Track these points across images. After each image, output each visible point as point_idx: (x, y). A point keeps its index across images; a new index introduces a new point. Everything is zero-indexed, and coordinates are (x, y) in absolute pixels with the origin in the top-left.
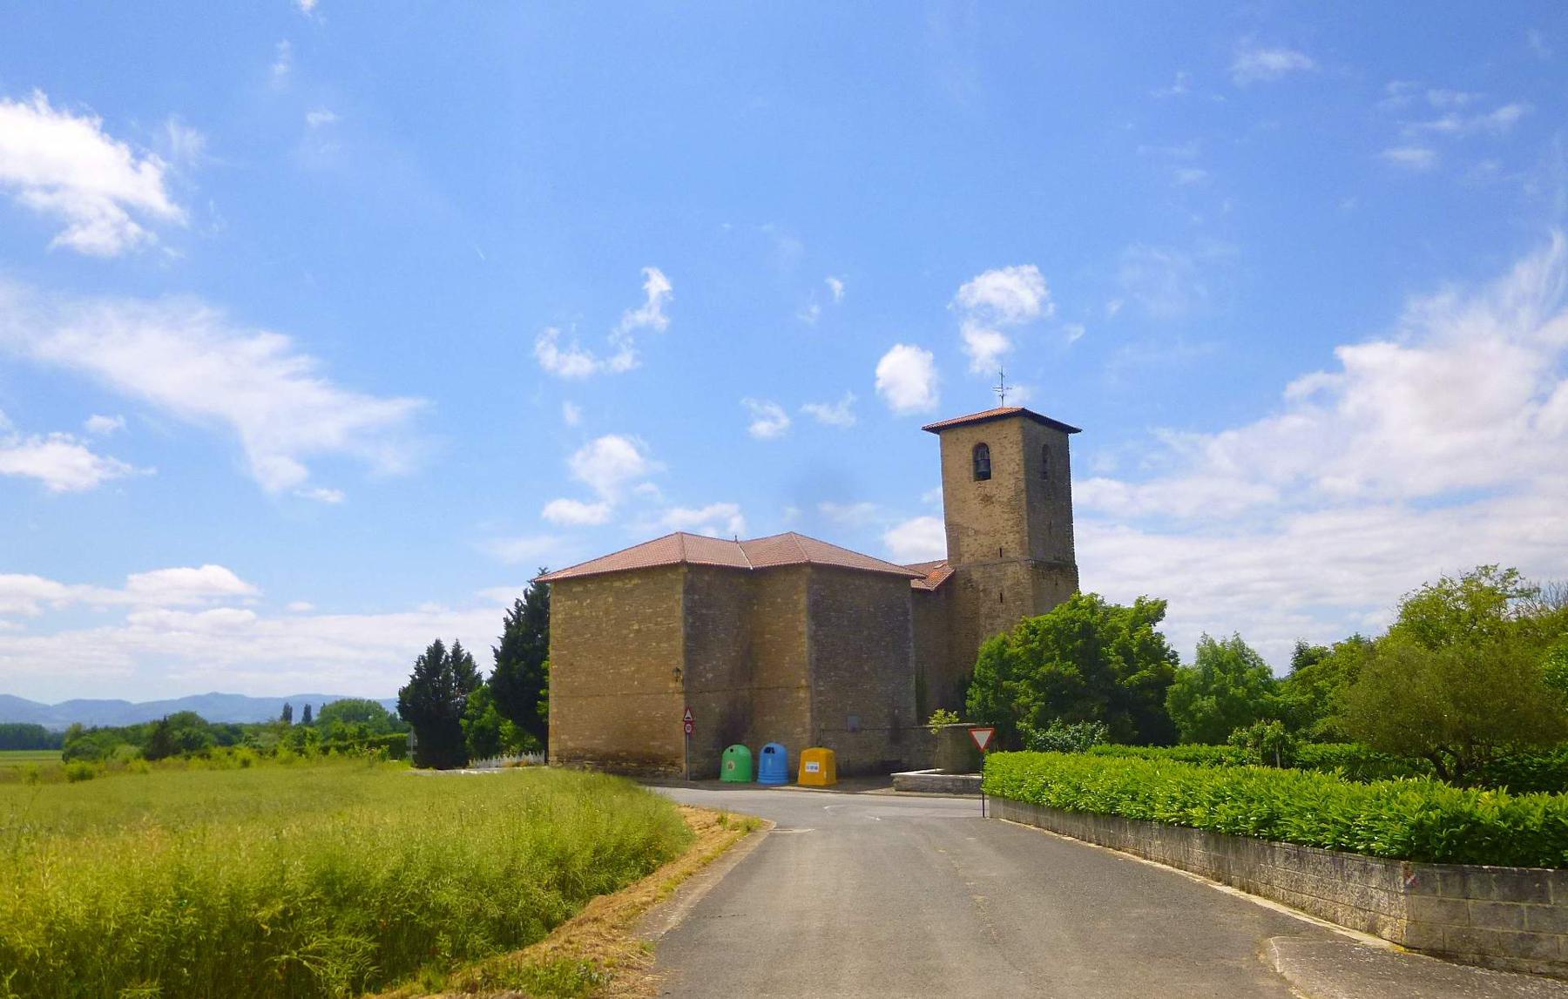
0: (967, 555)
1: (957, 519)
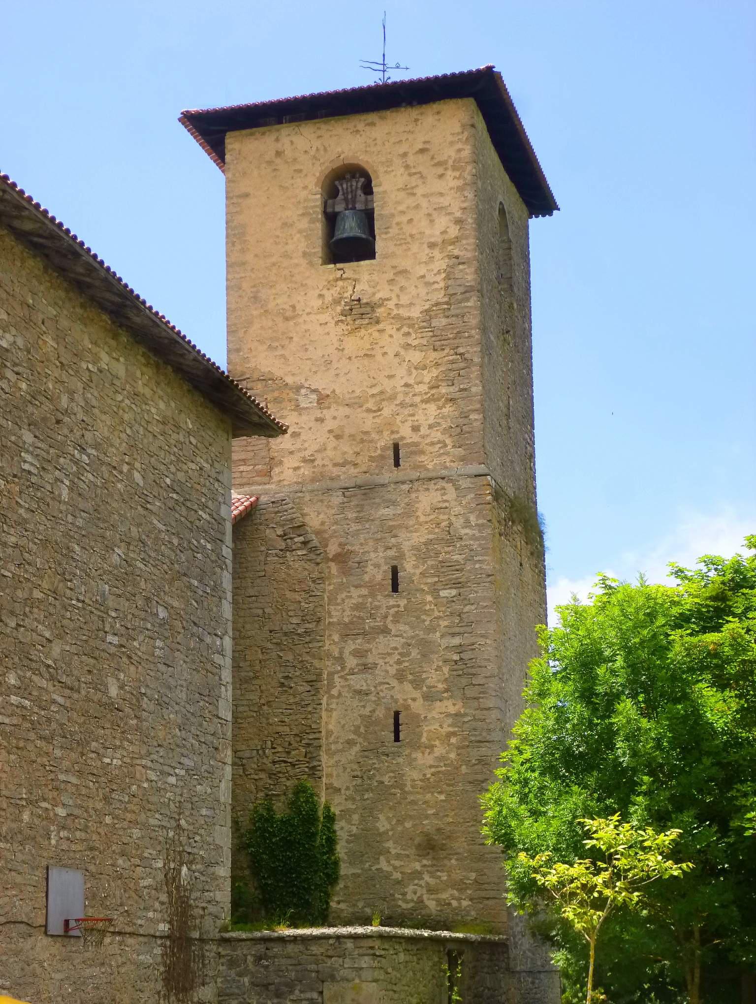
0: (290, 462)
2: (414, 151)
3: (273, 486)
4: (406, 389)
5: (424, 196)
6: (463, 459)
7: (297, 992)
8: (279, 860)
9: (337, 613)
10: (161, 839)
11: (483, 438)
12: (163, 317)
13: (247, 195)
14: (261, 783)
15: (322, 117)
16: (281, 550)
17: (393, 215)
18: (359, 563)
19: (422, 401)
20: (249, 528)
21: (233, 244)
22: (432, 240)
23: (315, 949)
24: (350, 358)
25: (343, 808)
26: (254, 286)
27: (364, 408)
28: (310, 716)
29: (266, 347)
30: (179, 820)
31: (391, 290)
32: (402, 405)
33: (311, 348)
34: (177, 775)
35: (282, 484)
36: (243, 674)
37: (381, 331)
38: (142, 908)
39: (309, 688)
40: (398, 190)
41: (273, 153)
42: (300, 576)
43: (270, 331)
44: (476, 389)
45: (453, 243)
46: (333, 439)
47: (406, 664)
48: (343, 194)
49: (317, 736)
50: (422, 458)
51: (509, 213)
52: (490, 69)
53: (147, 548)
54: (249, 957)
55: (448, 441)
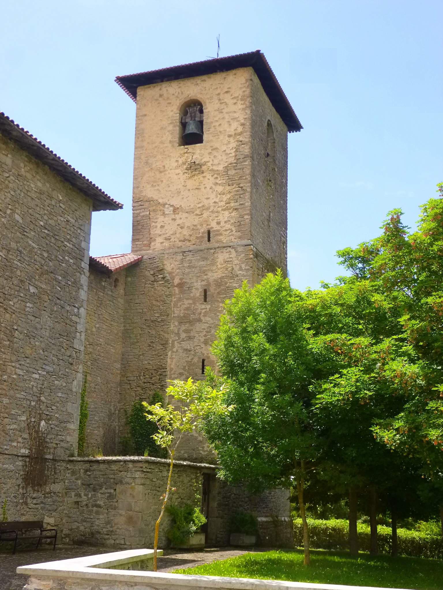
0: (159, 240)
1: (150, 193)
2: (223, 92)
3: (151, 251)
4: (215, 204)
5: (227, 113)
6: (240, 238)
7: (104, 489)
8: (144, 429)
9: (177, 312)
10: (24, 405)
11: (251, 227)
12: (27, 132)
13: (145, 115)
14: (138, 393)
15: (181, 78)
16: (152, 281)
17: (212, 122)
18: (189, 288)
19: (222, 210)
20: (138, 271)
21: (138, 138)
22: (230, 133)
23: (114, 467)
24: (189, 190)
25: (176, 405)
26: (147, 157)
27: (195, 214)
28: (162, 361)
29: (150, 185)
30: (40, 397)
31: (210, 158)
32: (212, 212)
33: (171, 185)
34: (39, 374)
35: (155, 250)
36: (132, 340)
37: (204, 177)
38: (8, 440)
39: (162, 347)
40: (215, 110)
41: (158, 95)
42: (160, 294)
43: (153, 178)
44: (248, 204)
45: (240, 135)
46: (179, 228)
47: (209, 337)
48: (190, 114)
49: (165, 370)
50: (221, 237)
51: (274, 126)
52: (258, 51)
53: (22, 255)
54: (81, 470)
55: (234, 229)
